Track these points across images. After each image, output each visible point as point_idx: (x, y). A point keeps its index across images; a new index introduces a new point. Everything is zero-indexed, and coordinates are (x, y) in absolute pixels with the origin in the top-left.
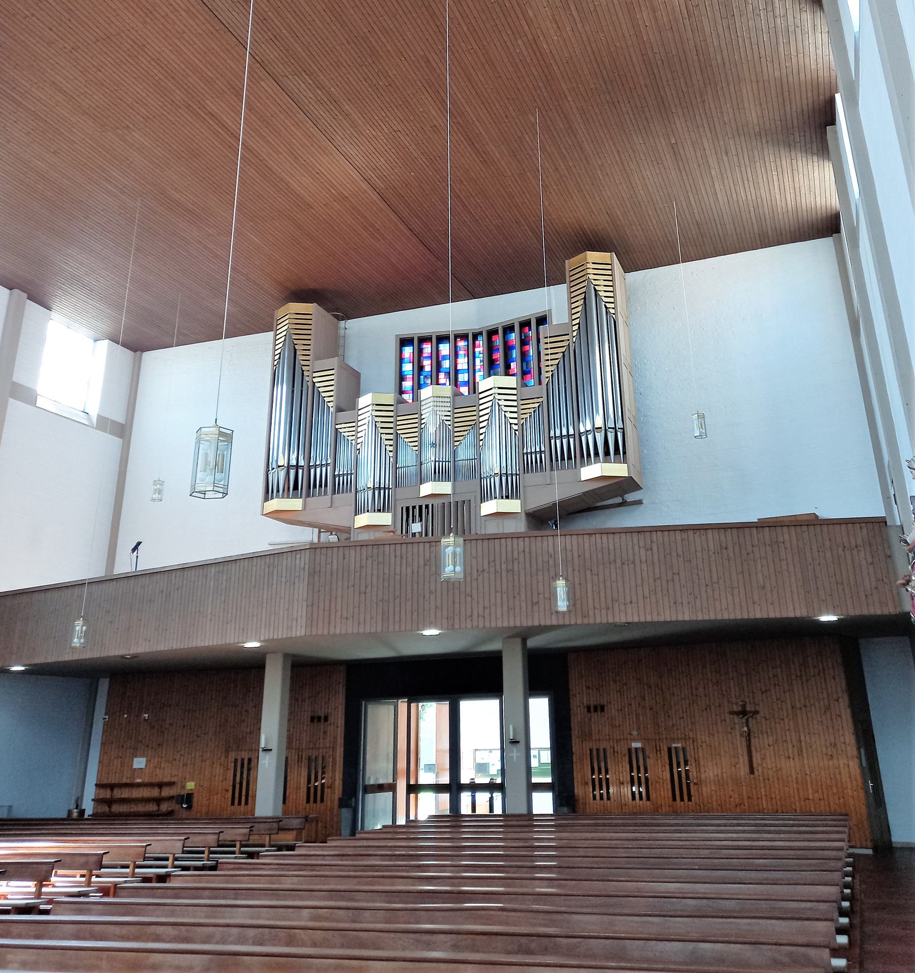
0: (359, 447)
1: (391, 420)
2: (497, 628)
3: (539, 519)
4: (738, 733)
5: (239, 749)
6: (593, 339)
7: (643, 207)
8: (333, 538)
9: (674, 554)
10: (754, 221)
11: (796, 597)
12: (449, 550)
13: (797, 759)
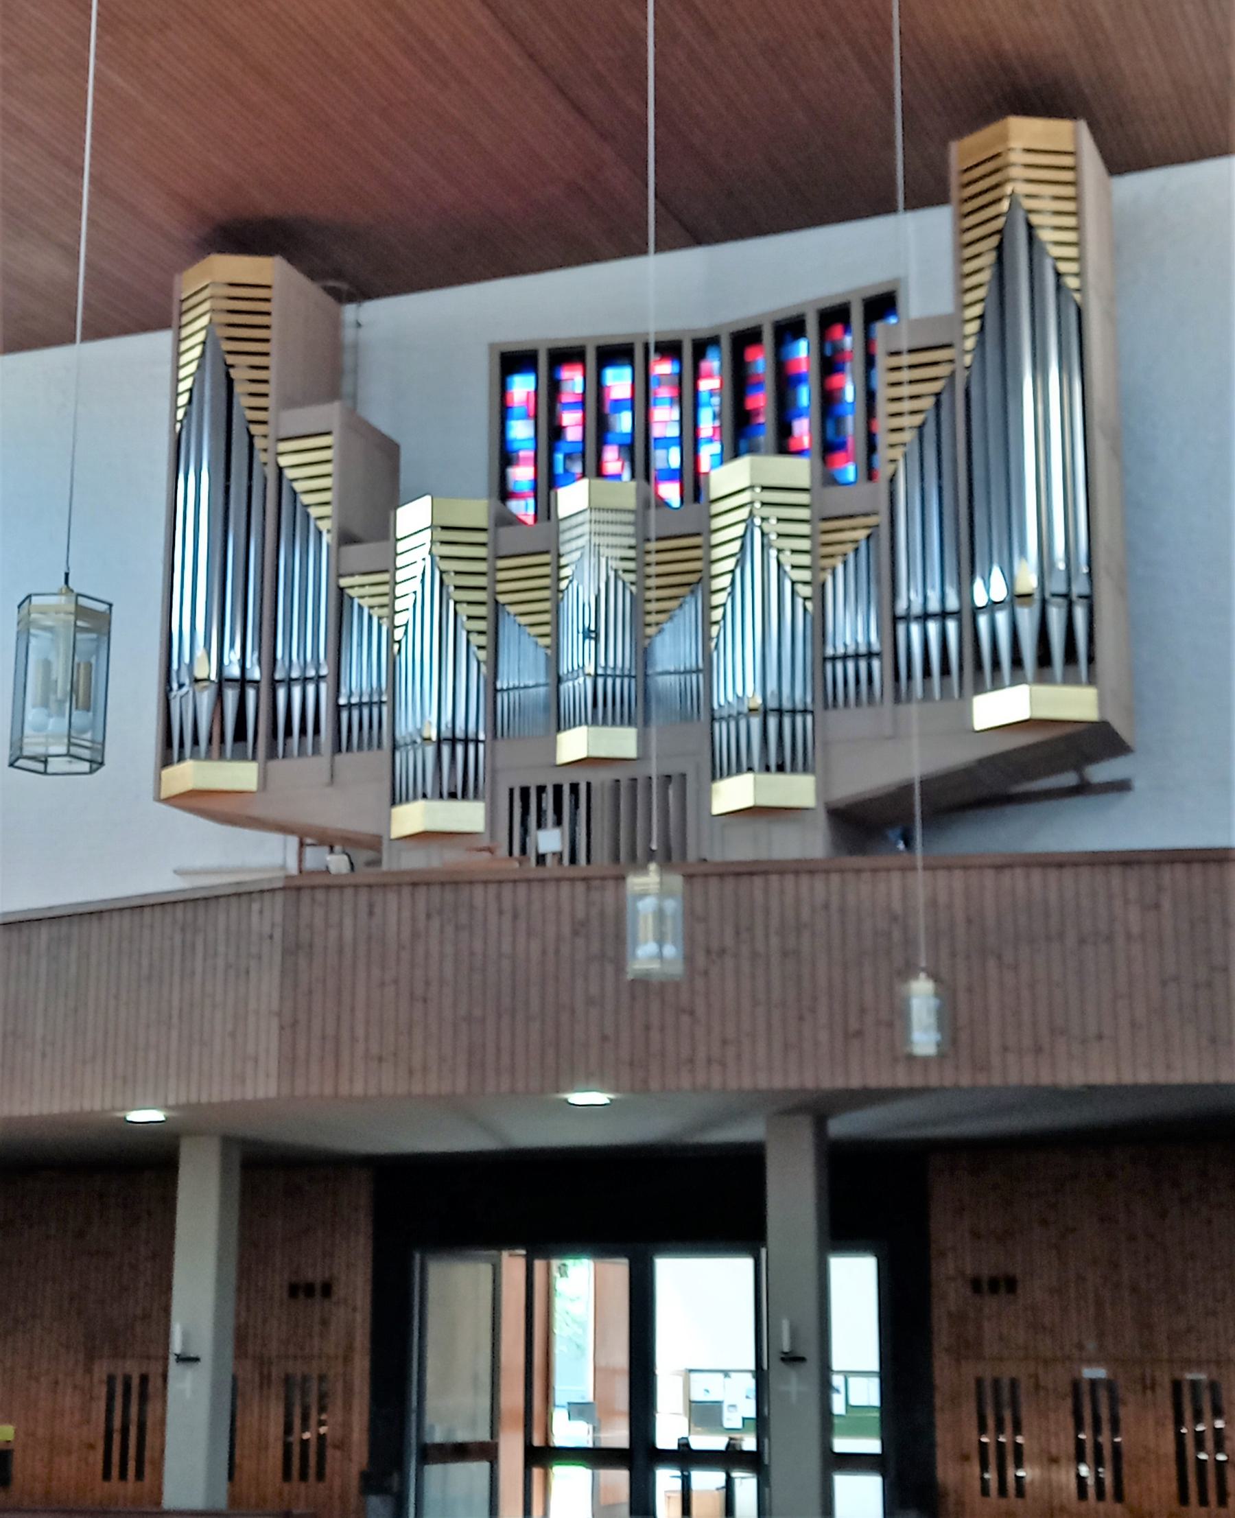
1: (481, 566)
2: (756, 1091)
3: (862, 825)
5: (118, 1354)
6: (1017, 325)
8: (337, 863)
12: (647, 906)
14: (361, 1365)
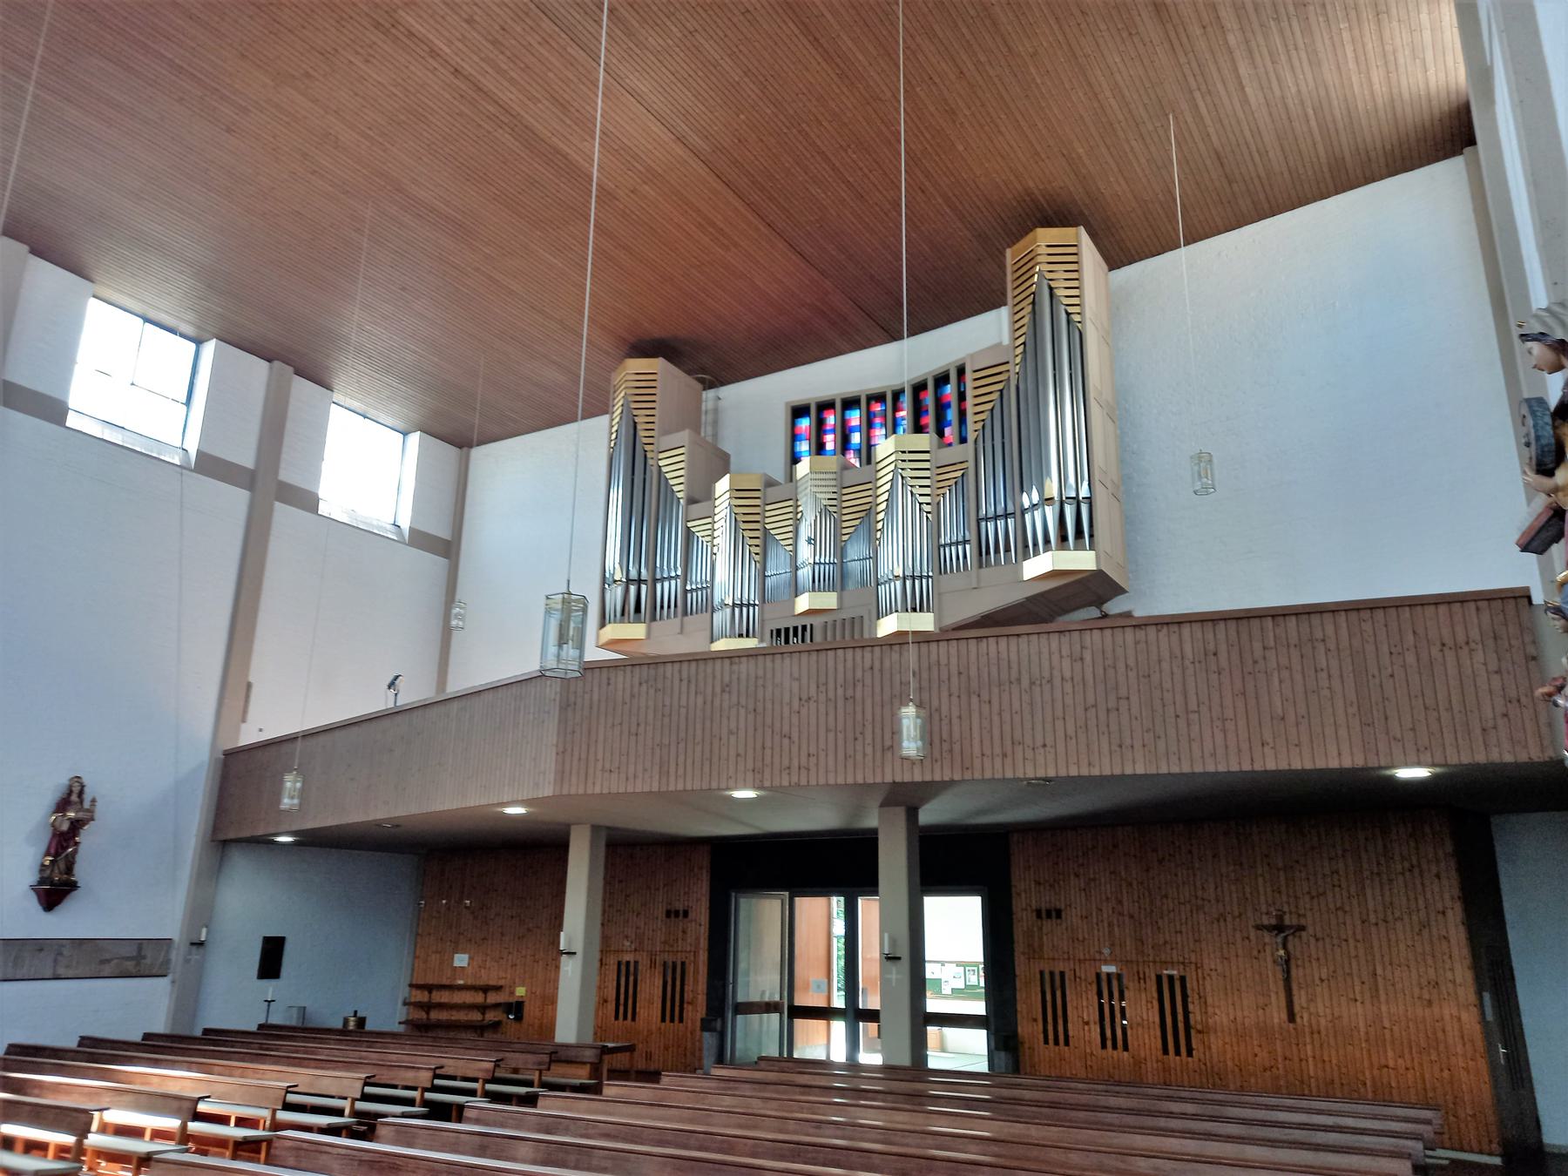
4: (1269, 959)
7: (1121, 134)
9: (1121, 666)
10: (1318, 139)
11: (1343, 732)
13: (1368, 1002)
14: (703, 957)
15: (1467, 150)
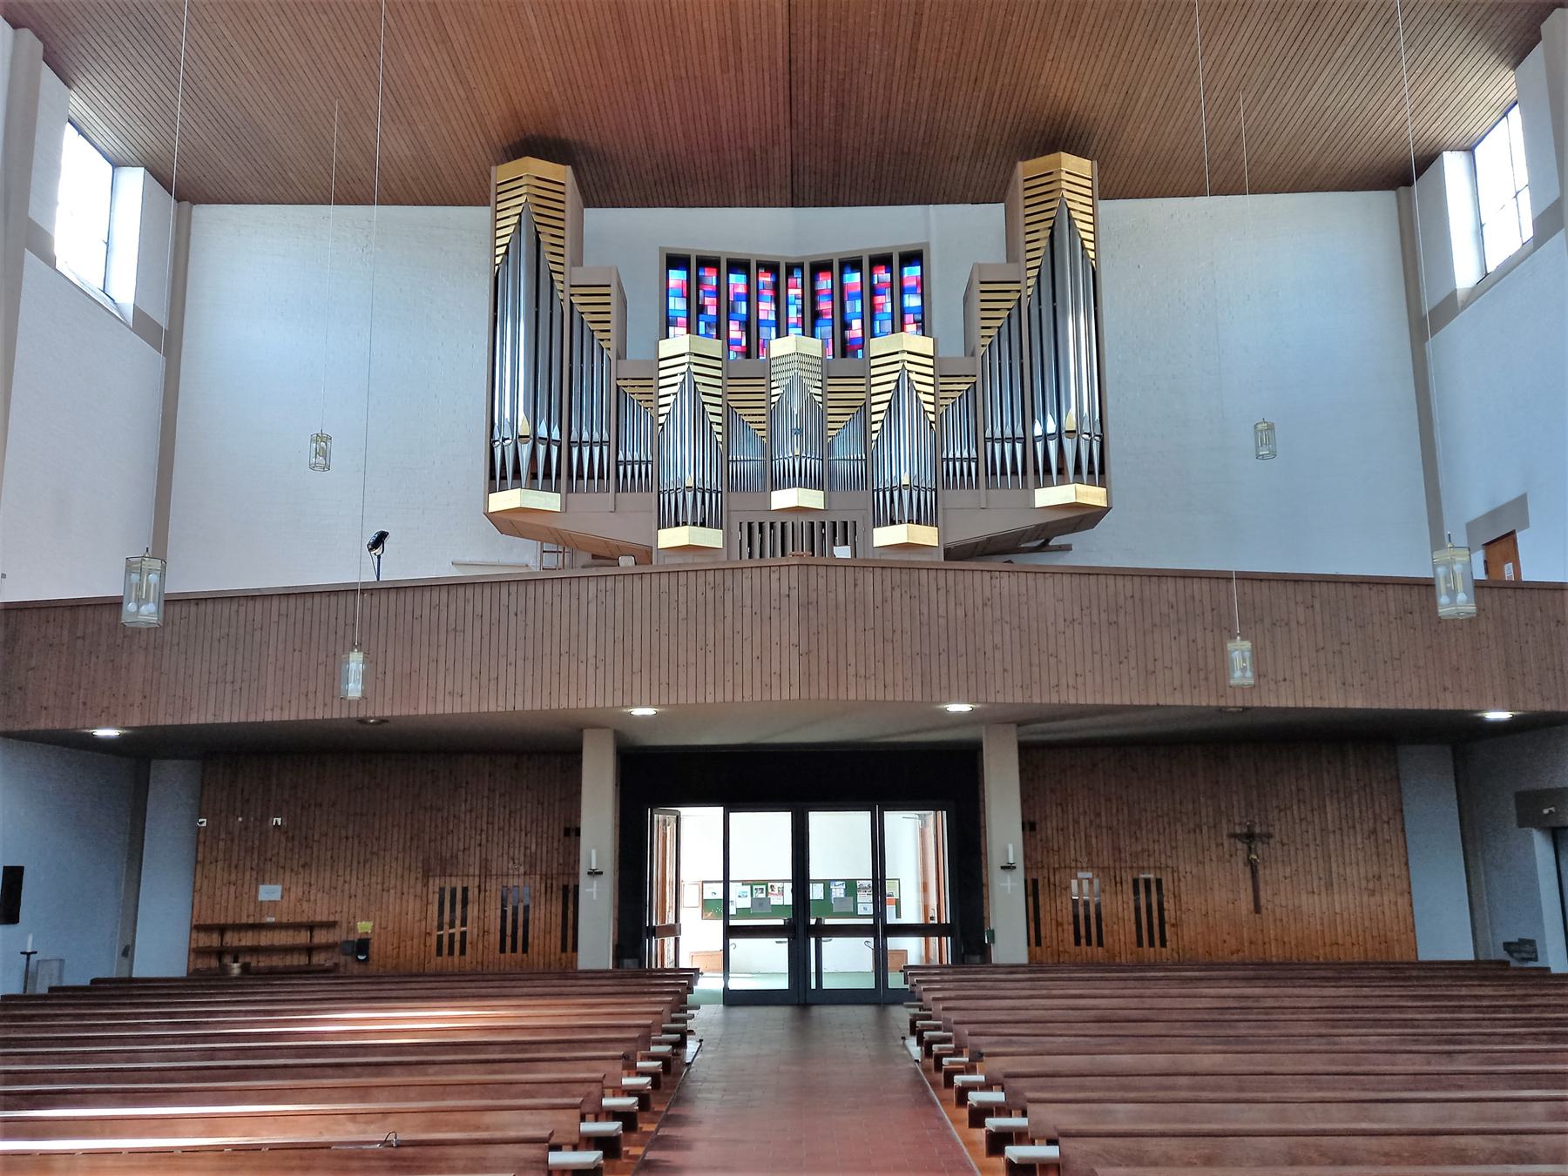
0: (662, 420)
5: (443, 874)
15: (1402, 189)
